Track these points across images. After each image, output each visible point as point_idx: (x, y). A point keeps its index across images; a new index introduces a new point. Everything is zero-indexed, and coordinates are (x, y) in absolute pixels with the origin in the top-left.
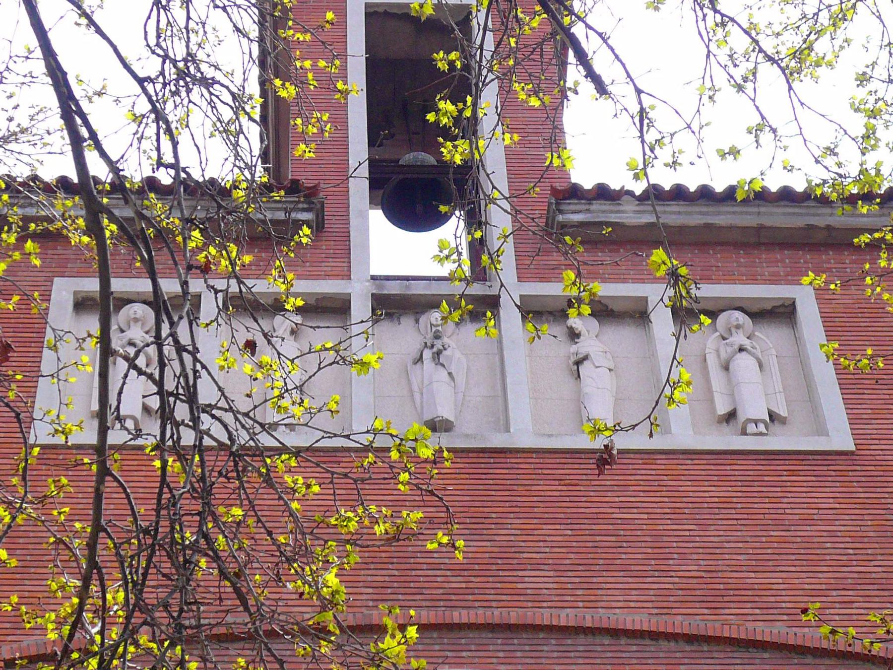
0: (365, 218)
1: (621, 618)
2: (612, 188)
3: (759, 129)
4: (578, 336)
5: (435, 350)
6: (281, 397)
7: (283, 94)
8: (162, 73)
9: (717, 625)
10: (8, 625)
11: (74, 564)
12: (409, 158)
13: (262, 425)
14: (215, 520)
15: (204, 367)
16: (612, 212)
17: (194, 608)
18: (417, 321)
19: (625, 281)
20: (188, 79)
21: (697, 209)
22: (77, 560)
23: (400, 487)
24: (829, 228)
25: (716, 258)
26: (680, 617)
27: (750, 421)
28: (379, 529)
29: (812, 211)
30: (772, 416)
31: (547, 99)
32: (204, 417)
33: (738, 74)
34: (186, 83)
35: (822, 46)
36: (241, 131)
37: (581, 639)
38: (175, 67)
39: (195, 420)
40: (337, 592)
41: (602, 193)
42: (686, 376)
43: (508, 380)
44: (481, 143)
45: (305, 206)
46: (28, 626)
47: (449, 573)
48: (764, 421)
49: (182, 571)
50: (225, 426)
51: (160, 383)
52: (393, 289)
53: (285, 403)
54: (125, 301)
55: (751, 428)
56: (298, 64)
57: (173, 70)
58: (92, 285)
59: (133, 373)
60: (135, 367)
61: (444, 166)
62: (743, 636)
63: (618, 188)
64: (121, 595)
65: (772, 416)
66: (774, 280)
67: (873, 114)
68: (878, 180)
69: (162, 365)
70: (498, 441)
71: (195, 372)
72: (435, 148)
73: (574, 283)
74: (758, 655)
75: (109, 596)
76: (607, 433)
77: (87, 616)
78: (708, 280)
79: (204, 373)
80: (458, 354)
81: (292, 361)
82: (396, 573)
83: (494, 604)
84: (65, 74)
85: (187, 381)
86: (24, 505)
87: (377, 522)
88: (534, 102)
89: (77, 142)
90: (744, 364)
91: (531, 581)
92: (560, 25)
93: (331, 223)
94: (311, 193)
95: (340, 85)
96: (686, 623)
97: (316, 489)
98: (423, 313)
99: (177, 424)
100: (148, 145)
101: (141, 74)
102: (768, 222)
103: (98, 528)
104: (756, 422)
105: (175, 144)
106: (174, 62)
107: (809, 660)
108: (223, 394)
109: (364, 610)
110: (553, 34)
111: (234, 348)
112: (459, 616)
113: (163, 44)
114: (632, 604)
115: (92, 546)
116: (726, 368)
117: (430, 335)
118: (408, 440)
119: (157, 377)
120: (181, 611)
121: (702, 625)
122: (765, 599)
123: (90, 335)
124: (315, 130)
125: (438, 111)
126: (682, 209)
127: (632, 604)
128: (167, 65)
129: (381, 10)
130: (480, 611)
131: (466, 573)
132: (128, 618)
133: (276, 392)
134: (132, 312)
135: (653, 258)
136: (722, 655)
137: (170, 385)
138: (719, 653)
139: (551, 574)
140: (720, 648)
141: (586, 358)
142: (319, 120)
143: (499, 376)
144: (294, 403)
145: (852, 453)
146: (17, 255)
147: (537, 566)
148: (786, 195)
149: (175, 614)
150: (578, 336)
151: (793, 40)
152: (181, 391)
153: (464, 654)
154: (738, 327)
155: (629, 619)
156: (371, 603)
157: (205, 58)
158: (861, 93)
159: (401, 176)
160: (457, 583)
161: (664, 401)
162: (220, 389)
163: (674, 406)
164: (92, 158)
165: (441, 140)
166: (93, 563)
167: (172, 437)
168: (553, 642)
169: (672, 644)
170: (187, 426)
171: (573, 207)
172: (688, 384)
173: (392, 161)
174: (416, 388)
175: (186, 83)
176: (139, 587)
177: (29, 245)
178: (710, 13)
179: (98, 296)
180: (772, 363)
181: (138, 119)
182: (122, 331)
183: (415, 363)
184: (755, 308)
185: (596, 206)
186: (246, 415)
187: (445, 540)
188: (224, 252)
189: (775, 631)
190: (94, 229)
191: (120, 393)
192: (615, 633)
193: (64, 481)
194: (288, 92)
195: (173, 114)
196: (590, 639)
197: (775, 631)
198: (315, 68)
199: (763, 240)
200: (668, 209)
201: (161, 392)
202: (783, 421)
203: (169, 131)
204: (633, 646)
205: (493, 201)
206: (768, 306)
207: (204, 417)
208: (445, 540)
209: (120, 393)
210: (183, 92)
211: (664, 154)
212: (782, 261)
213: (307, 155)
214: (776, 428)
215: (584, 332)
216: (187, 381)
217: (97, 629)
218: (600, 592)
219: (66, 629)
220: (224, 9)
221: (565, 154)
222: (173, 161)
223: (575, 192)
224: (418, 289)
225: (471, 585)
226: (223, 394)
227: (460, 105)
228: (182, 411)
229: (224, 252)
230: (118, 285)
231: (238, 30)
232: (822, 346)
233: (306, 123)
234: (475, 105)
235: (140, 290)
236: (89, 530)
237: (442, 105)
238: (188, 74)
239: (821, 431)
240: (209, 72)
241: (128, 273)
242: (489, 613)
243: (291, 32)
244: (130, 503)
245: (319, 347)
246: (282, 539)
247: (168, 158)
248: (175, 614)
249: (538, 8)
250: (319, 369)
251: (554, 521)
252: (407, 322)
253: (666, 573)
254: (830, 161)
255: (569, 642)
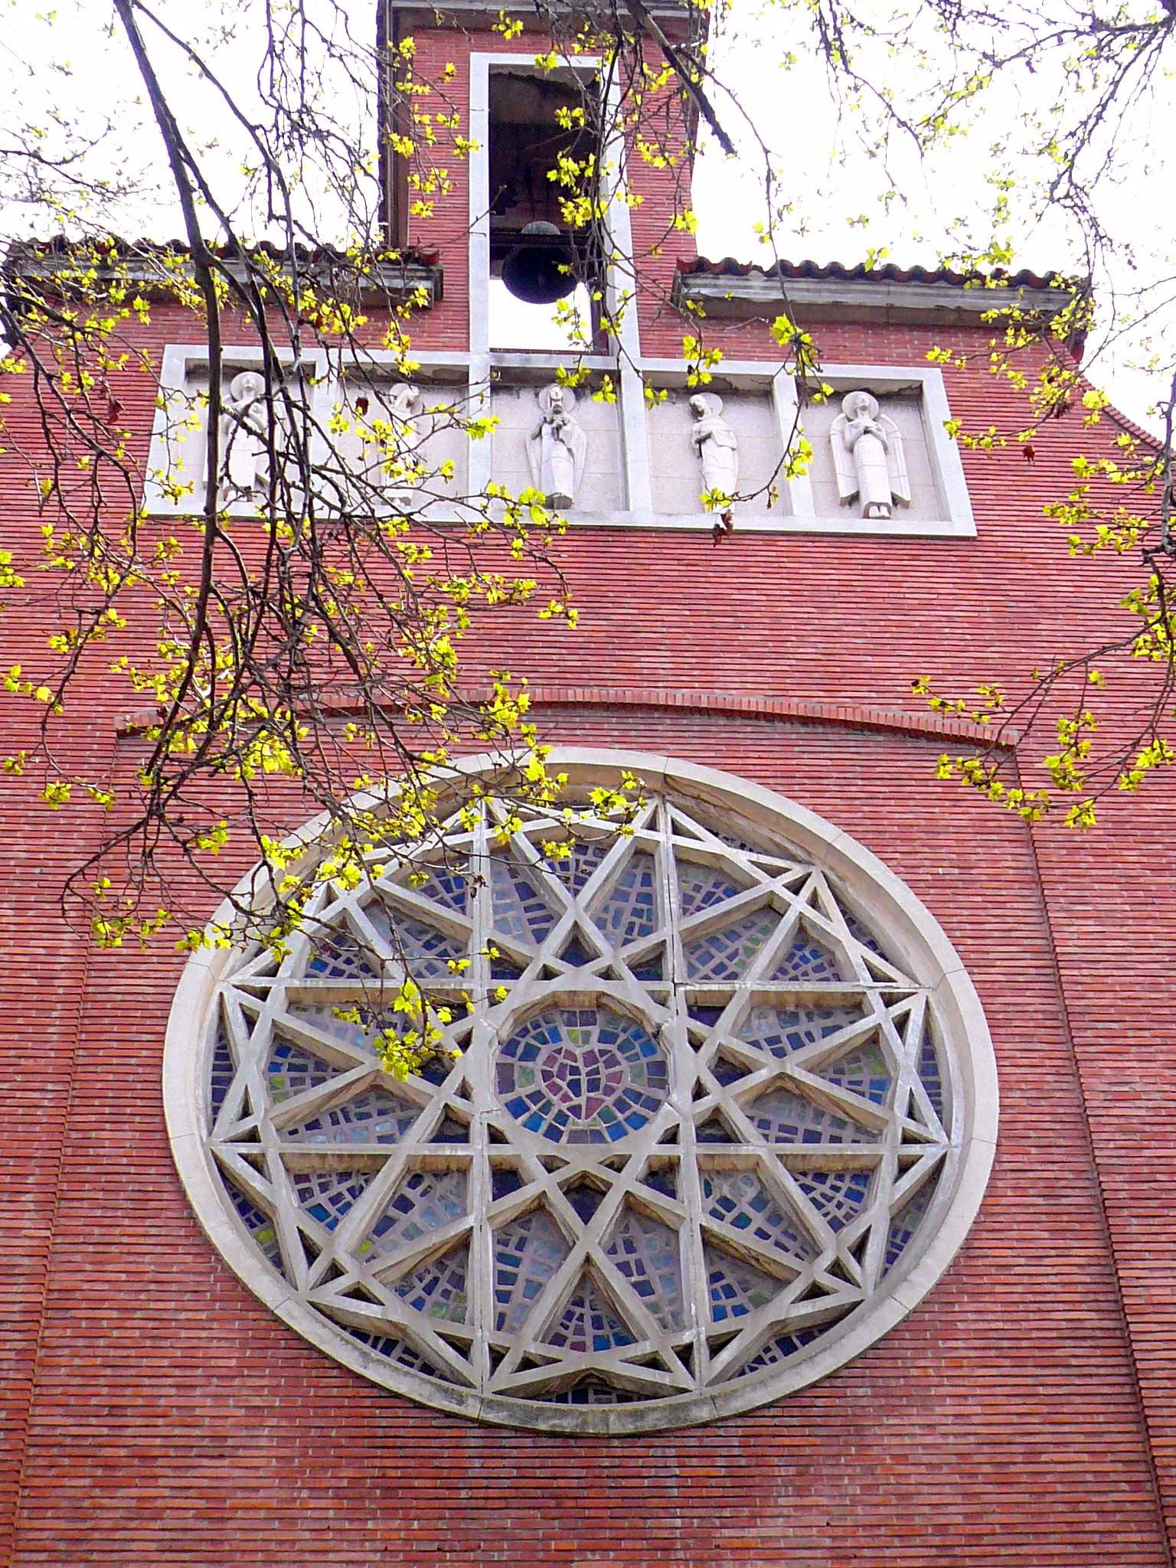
0: (482, 285)
1: (737, 700)
2: (740, 262)
3: (890, 197)
4: (701, 414)
5: (554, 425)
6: (394, 460)
7: (400, 148)
8: (276, 125)
9: (834, 707)
10: (121, 696)
11: (183, 624)
12: (532, 227)
13: (374, 489)
14: (325, 582)
15: (314, 423)
16: (739, 287)
17: (304, 669)
18: (537, 395)
19: (750, 358)
20: (302, 131)
21: (827, 286)
22: (186, 621)
23: (513, 553)
24: (959, 310)
25: (844, 338)
26: (796, 700)
27: (872, 504)
28: (492, 597)
29: (942, 292)
30: (895, 500)
31: (672, 161)
32: (314, 477)
33: (871, 140)
34: (301, 136)
35: (958, 114)
36: (356, 186)
37: (697, 719)
38: (289, 118)
39: (305, 479)
40: (448, 655)
41: (730, 268)
42: (806, 448)
43: (629, 458)
44: (603, 204)
45: (424, 274)
46: (138, 688)
47: (564, 651)
48: (886, 505)
49: (290, 630)
50: (336, 488)
51: (270, 443)
52: (513, 361)
53: (396, 467)
54: (236, 370)
55: (874, 511)
56: (417, 118)
57: (288, 122)
58: (202, 352)
59: (241, 432)
60: (245, 426)
61: (567, 229)
62: (858, 719)
63: (745, 263)
64: (230, 659)
65: (895, 500)
66: (902, 361)
67: (1006, 186)
68: (1007, 254)
69: (272, 423)
70: (617, 519)
71: (305, 429)
72: (555, 215)
73: (695, 349)
74: (873, 738)
75: (219, 660)
76: (726, 503)
77: (197, 681)
78: (835, 359)
79: (314, 430)
80: (578, 430)
81: (405, 423)
82: (511, 650)
83: (609, 683)
84: (173, 120)
85: (297, 442)
86: (133, 567)
87: (489, 589)
88: (659, 163)
89: (185, 190)
90: (869, 447)
91: (647, 661)
92: (689, 81)
93: (450, 292)
94: (428, 261)
95: (459, 141)
96: (802, 705)
97: (428, 554)
98: (543, 387)
99: (287, 486)
100: (261, 199)
101: (253, 123)
102: (898, 302)
103: (206, 588)
104: (879, 505)
105: (286, 196)
106: (288, 114)
107: (923, 743)
108: (334, 452)
109: (477, 686)
110: (680, 90)
111: (347, 410)
112: (573, 695)
113: (276, 94)
114: (749, 686)
115: (201, 606)
116: (851, 450)
117: (550, 410)
118: (521, 504)
119: (267, 436)
120: (291, 672)
121: (817, 707)
122: (881, 682)
123: (200, 395)
124: (433, 188)
125: (559, 169)
126: (811, 286)
127: (749, 686)
128: (281, 115)
129: (505, 72)
130: (595, 690)
131: (582, 652)
132: (237, 679)
133: (389, 456)
134: (244, 381)
135: (775, 326)
136: (836, 737)
137: (279, 445)
138: (834, 736)
139: (668, 654)
140: (835, 730)
141: (709, 436)
142: (437, 177)
143: (619, 452)
144: (407, 469)
145: (974, 539)
146: (126, 312)
147: (653, 645)
148: (918, 275)
149: (285, 675)
150: (701, 414)
151: (927, 108)
152: (291, 451)
153: (578, 732)
154: (864, 408)
155: (745, 700)
156: (485, 680)
157: (320, 110)
158: (995, 164)
159: (524, 246)
160: (573, 662)
161: (783, 471)
162: (331, 447)
163: (793, 477)
164: (203, 213)
165: (562, 200)
166: (202, 625)
167: (282, 497)
168: (668, 721)
169: (788, 725)
170: (298, 488)
171: (699, 281)
172: (809, 454)
173: (512, 230)
174: (534, 464)
175: (301, 136)
176: (249, 644)
177: (138, 303)
178: (842, 74)
179: (208, 363)
180: (898, 446)
181: (250, 172)
182: (235, 400)
183: (534, 438)
184: (881, 390)
185: (723, 280)
186: (359, 477)
187: (559, 608)
188: (338, 313)
189: (890, 714)
190: (206, 286)
191: (229, 449)
192: (729, 714)
193: (173, 541)
194: (406, 147)
195: (288, 169)
196: (705, 720)
197: (890, 714)
198: (434, 122)
199: (893, 321)
200: (796, 285)
201: (270, 450)
202: (906, 505)
203: (281, 181)
204: (748, 728)
205: (614, 262)
206: (895, 388)
207: (314, 477)
208: (559, 608)
209: (229, 449)
210: (296, 143)
211: (791, 221)
212: (910, 342)
213: (425, 214)
214: (899, 511)
215: (707, 410)
216: (297, 442)
217: (208, 692)
218: (716, 673)
219: (176, 692)
220: (341, 58)
221: (689, 216)
222: (284, 213)
223: (701, 266)
224: (539, 362)
225: (587, 664)
226: (334, 452)
227: (583, 164)
228: (292, 473)
229: (338, 313)
230: (230, 353)
231: (354, 80)
232: (945, 423)
233: (424, 179)
234: (597, 161)
235: (253, 358)
236: (198, 595)
237: (563, 163)
238: (303, 127)
239: (945, 517)
240: (324, 125)
241: (240, 341)
242: (604, 692)
243: (409, 85)
244: (242, 570)
245: (432, 409)
246: (393, 606)
247: (279, 209)
248: (285, 675)
249: (665, 64)
250: (433, 432)
251: (671, 601)
252: (526, 396)
253: (781, 655)
254: (960, 232)
255: (685, 722)
